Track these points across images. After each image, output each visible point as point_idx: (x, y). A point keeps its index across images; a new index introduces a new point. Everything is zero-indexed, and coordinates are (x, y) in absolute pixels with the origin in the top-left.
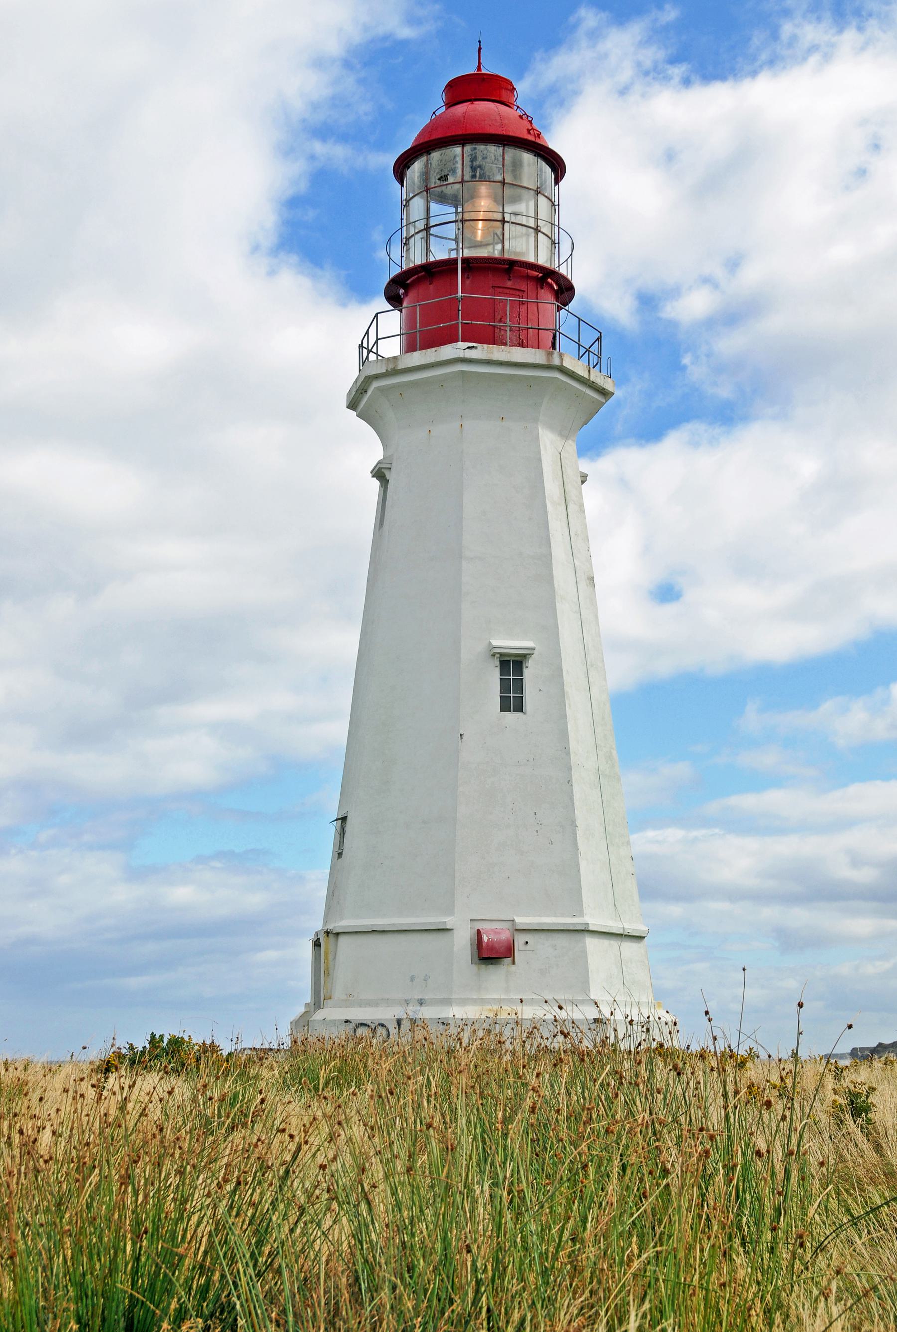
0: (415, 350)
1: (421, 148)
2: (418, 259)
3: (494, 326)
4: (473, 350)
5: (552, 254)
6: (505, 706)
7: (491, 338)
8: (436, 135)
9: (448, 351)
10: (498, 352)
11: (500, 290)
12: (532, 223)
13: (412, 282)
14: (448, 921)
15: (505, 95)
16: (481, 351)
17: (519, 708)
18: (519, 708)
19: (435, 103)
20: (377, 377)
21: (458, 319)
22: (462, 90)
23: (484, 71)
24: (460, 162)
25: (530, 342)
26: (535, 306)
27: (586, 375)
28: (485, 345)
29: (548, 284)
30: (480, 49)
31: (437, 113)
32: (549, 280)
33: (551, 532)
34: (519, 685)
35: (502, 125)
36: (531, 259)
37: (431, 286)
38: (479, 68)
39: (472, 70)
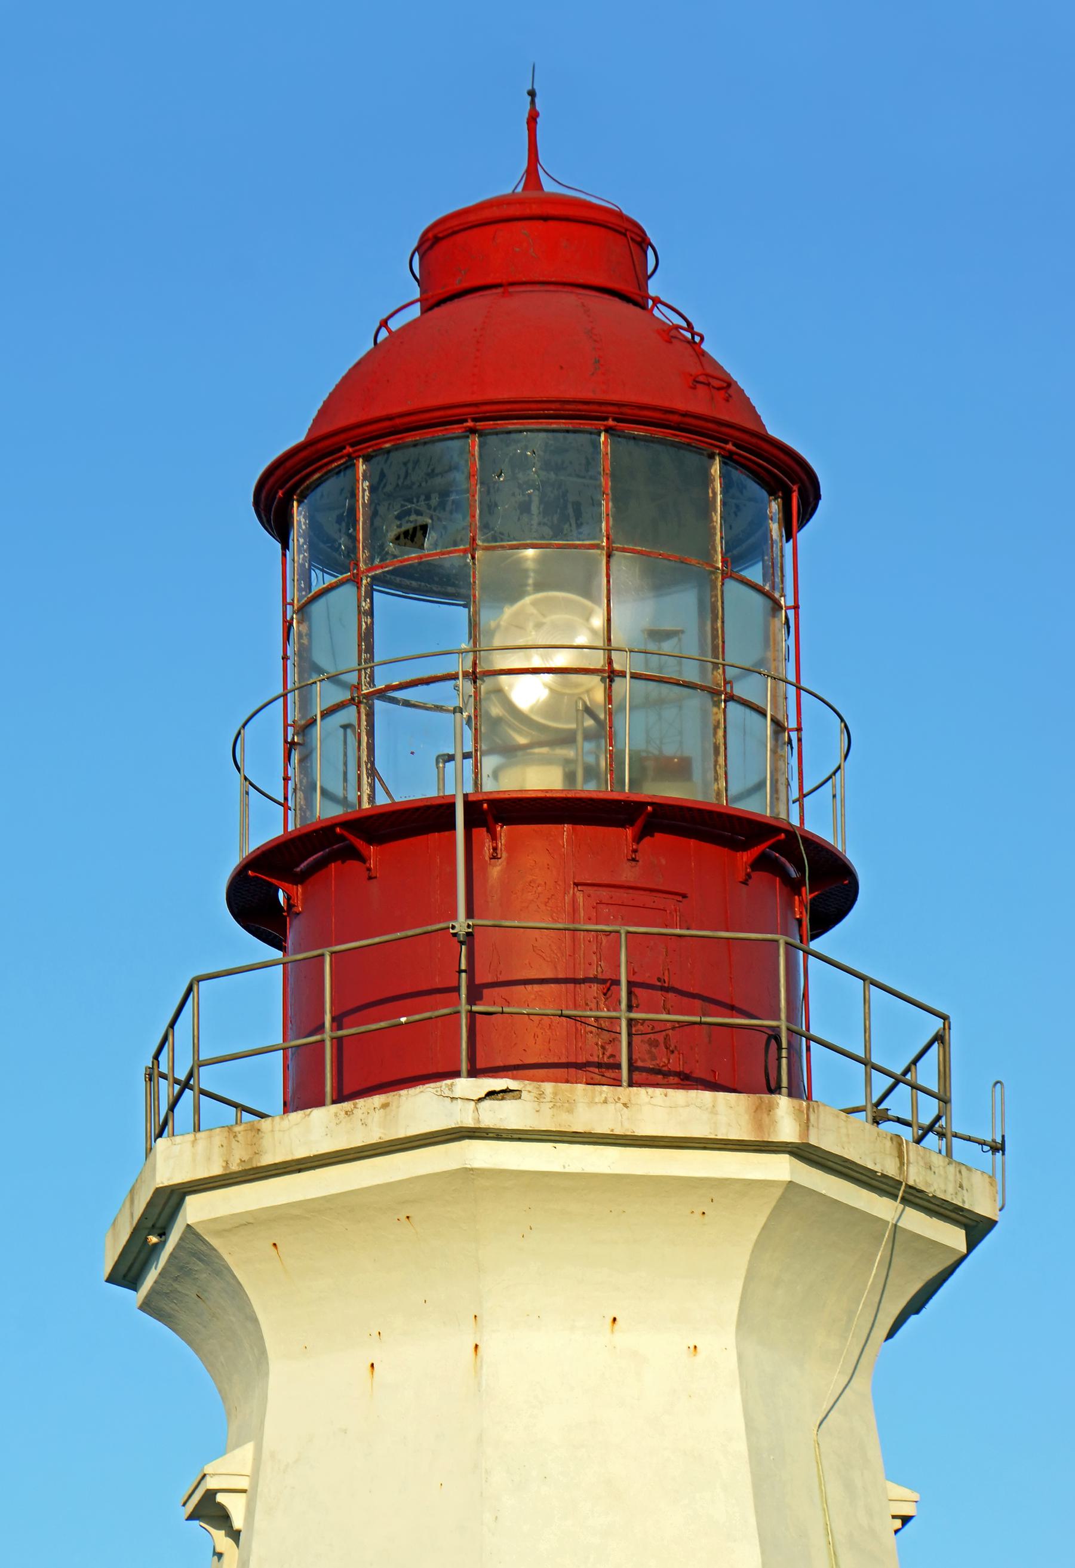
0: (320, 1103)
9: (423, 1107)
24: (636, 263)
27: (890, 1168)
30: (533, 118)
31: (395, 324)
39: (507, 182)
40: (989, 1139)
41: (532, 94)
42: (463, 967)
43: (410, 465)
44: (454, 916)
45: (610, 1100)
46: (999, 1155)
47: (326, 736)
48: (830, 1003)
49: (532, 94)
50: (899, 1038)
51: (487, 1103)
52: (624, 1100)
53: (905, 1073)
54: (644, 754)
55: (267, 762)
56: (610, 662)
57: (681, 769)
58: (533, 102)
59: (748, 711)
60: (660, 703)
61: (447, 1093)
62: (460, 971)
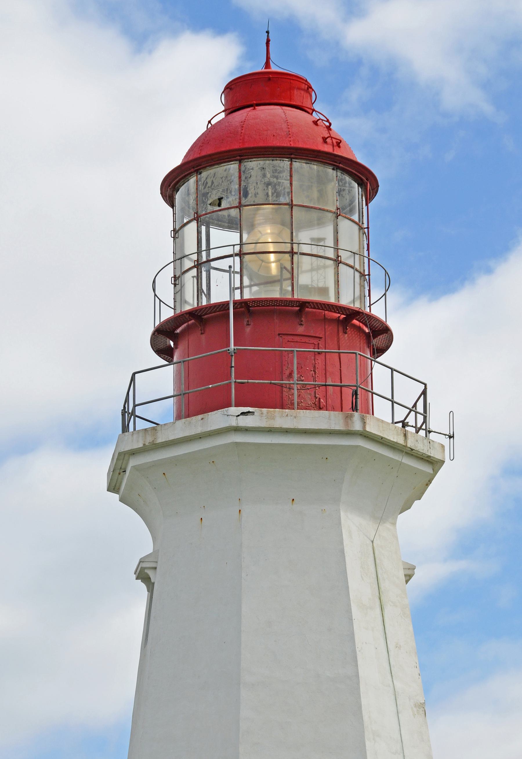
1: (196, 162)
2: (191, 302)
3: (281, 386)
4: (249, 418)
5: (362, 287)
7: (279, 401)
8: (208, 151)
9: (217, 419)
10: (281, 418)
11: (290, 338)
12: (330, 253)
13: (182, 332)
15: (298, 97)
16: (259, 417)
20: (133, 453)
21: (230, 378)
23: (274, 68)
25: (329, 401)
26: (336, 356)
27: (400, 440)
28: (264, 410)
29: (354, 326)
31: (213, 122)
32: (355, 322)
33: (358, 645)
35: (289, 134)
36: (332, 300)
37: (203, 336)
38: (267, 65)
39: (260, 68)
40: (448, 434)
41: (268, 32)
42: (233, 365)
43: (224, 179)
44: (229, 346)
45: (289, 415)
46: (452, 439)
47: (189, 280)
48: (380, 378)
49: (268, 32)
50: (407, 392)
51: (241, 416)
52: (295, 415)
53: (413, 407)
54: (310, 286)
55: (166, 291)
56: (292, 249)
57: (324, 290)
58: (268, 36)
59: (348, 267)
60: (318, 268)
61: (226, 413)
62: (232, 367)
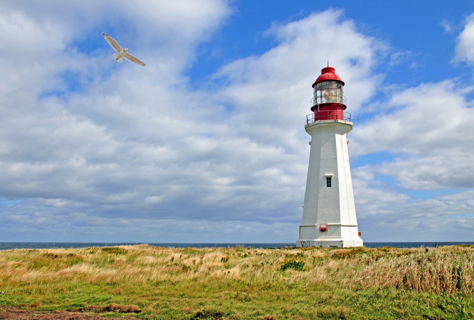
6: (328, 186)
7: (326, 118)
14: (316, 225)
16: (322, 121)
17: (330, 186)
18: (330, 186)
19: (320, 73)
22: (325, 71)
34: (330, 182)
39: (327, 67)
